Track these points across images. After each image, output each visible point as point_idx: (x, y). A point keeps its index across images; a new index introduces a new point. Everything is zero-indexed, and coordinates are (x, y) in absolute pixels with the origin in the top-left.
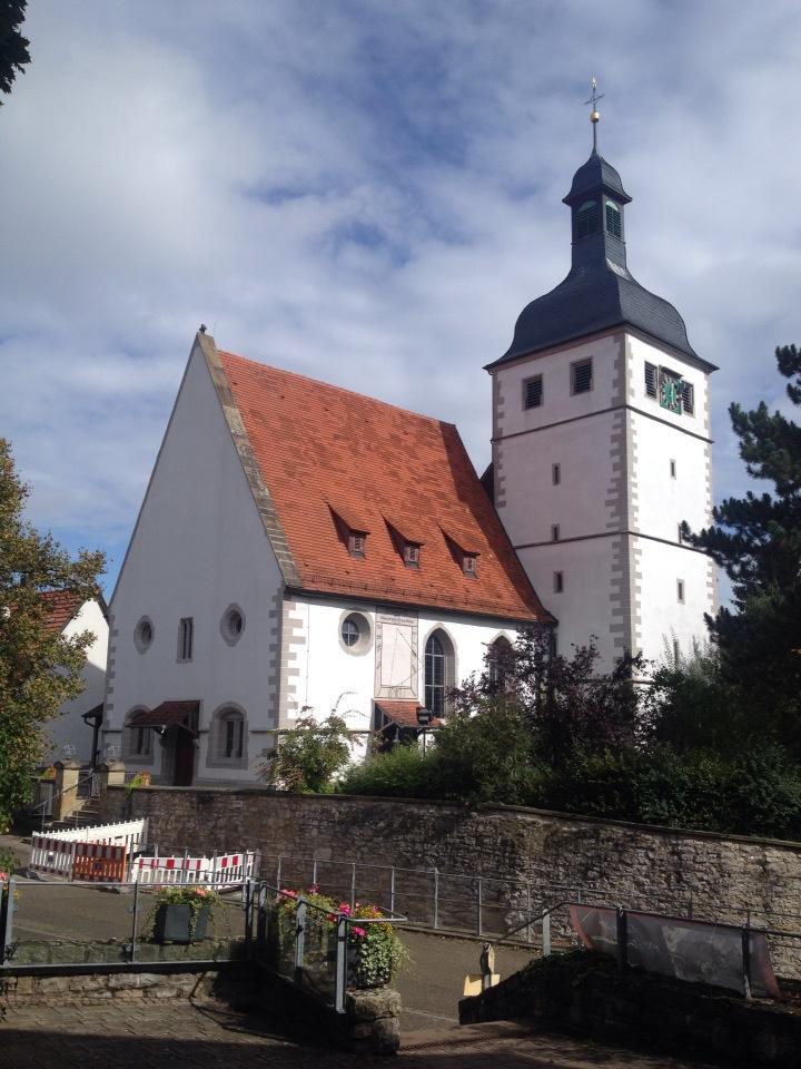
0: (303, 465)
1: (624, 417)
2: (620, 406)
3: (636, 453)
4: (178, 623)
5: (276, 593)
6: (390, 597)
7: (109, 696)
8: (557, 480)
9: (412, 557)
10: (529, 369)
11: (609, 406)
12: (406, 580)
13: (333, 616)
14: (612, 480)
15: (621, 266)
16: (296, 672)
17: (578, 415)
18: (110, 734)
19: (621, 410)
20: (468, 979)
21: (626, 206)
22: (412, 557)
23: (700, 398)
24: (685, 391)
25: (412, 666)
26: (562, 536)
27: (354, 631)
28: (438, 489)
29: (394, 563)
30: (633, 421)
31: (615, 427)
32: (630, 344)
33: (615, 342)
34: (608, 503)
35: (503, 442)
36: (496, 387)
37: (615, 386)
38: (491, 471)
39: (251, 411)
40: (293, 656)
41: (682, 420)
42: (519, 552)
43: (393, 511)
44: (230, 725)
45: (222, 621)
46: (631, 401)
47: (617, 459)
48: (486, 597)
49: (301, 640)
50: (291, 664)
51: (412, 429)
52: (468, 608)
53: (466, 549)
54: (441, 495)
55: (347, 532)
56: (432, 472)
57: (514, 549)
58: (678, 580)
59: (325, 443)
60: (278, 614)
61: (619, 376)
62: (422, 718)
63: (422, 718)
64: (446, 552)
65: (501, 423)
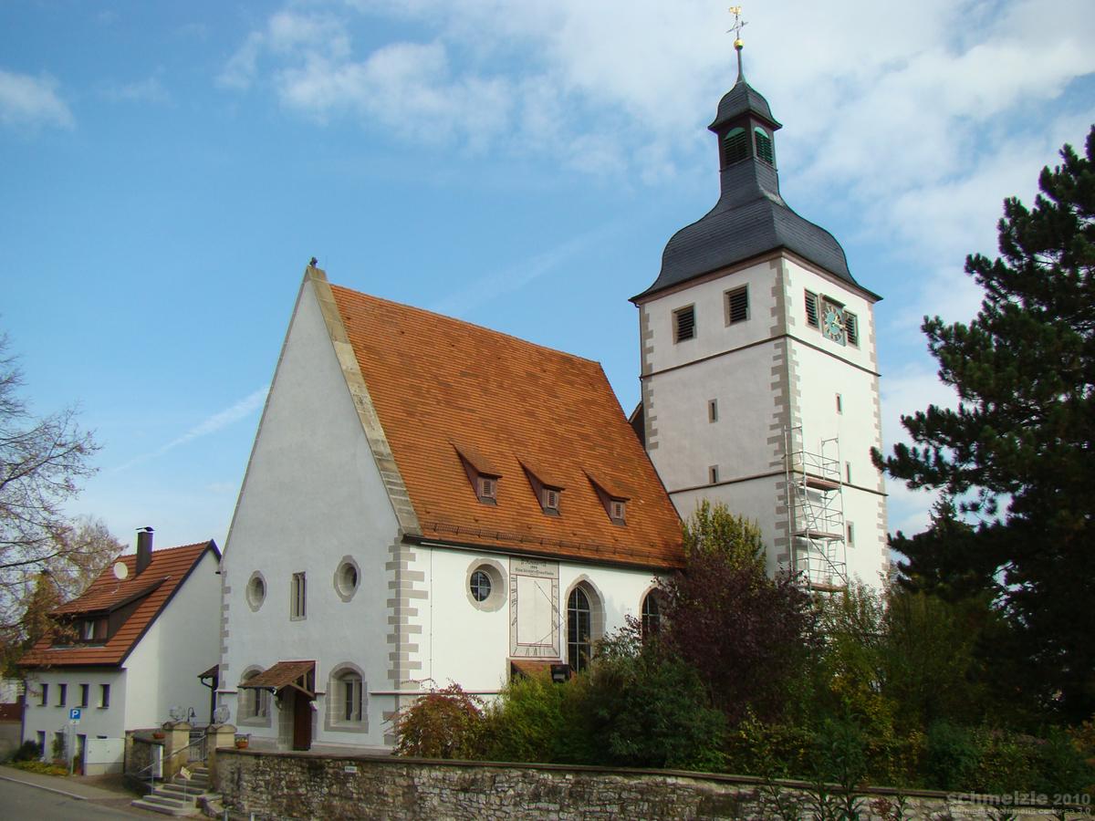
0: (423, 404)
1: (784, 347)
2: (780, 336)
3: (799, 386)
4: (290, 579)
5: (393, 544)
6: (525, 546)
7: (224, 655)
8: (714, 417)
9: (552, 503)
11: (769, 337)
12: (545, 529)
13: (459, 566)
14: (775, 416)
16: (418, 629)
18: (226, 695)
19: (782, 340)
20: (1038, 209)
21: (775, 132)
22: (552, 503)
23: (864, 329)
24: (849, 324)
25: (553, 622)
26: (721, 479)
27: (481, 585)
28: (583, 431)
29: (530, 509)
30: (795, 352)
31: (776, 358)
33: (771, 268)
34: (771, 440)
35: (654, 378)
36: (644, 320)
37: (773, 315)
38: (640, 413)
39: (366, 347)
40: (414, 612)
41: (846, 351)
42: (671, 496)
43: (529, 453)
44: (349, 686)
45: (335, 575)
46: (792, 331)
47: (778, 392)
48: (638, 546)
49: (423, 595)
50: (412, 621)
51: (552, 367)
52: (617, 558)
53: (614, 494)
54: (585, 437)
55: (475, 474)
56: (573, 411)
58: (853, 546)
59: (451, 380)
60: (394, 565)
61: (778, 302)
62: (556, 677)
63: (556, 677)
64: (592, 497)
65: (650, 358)
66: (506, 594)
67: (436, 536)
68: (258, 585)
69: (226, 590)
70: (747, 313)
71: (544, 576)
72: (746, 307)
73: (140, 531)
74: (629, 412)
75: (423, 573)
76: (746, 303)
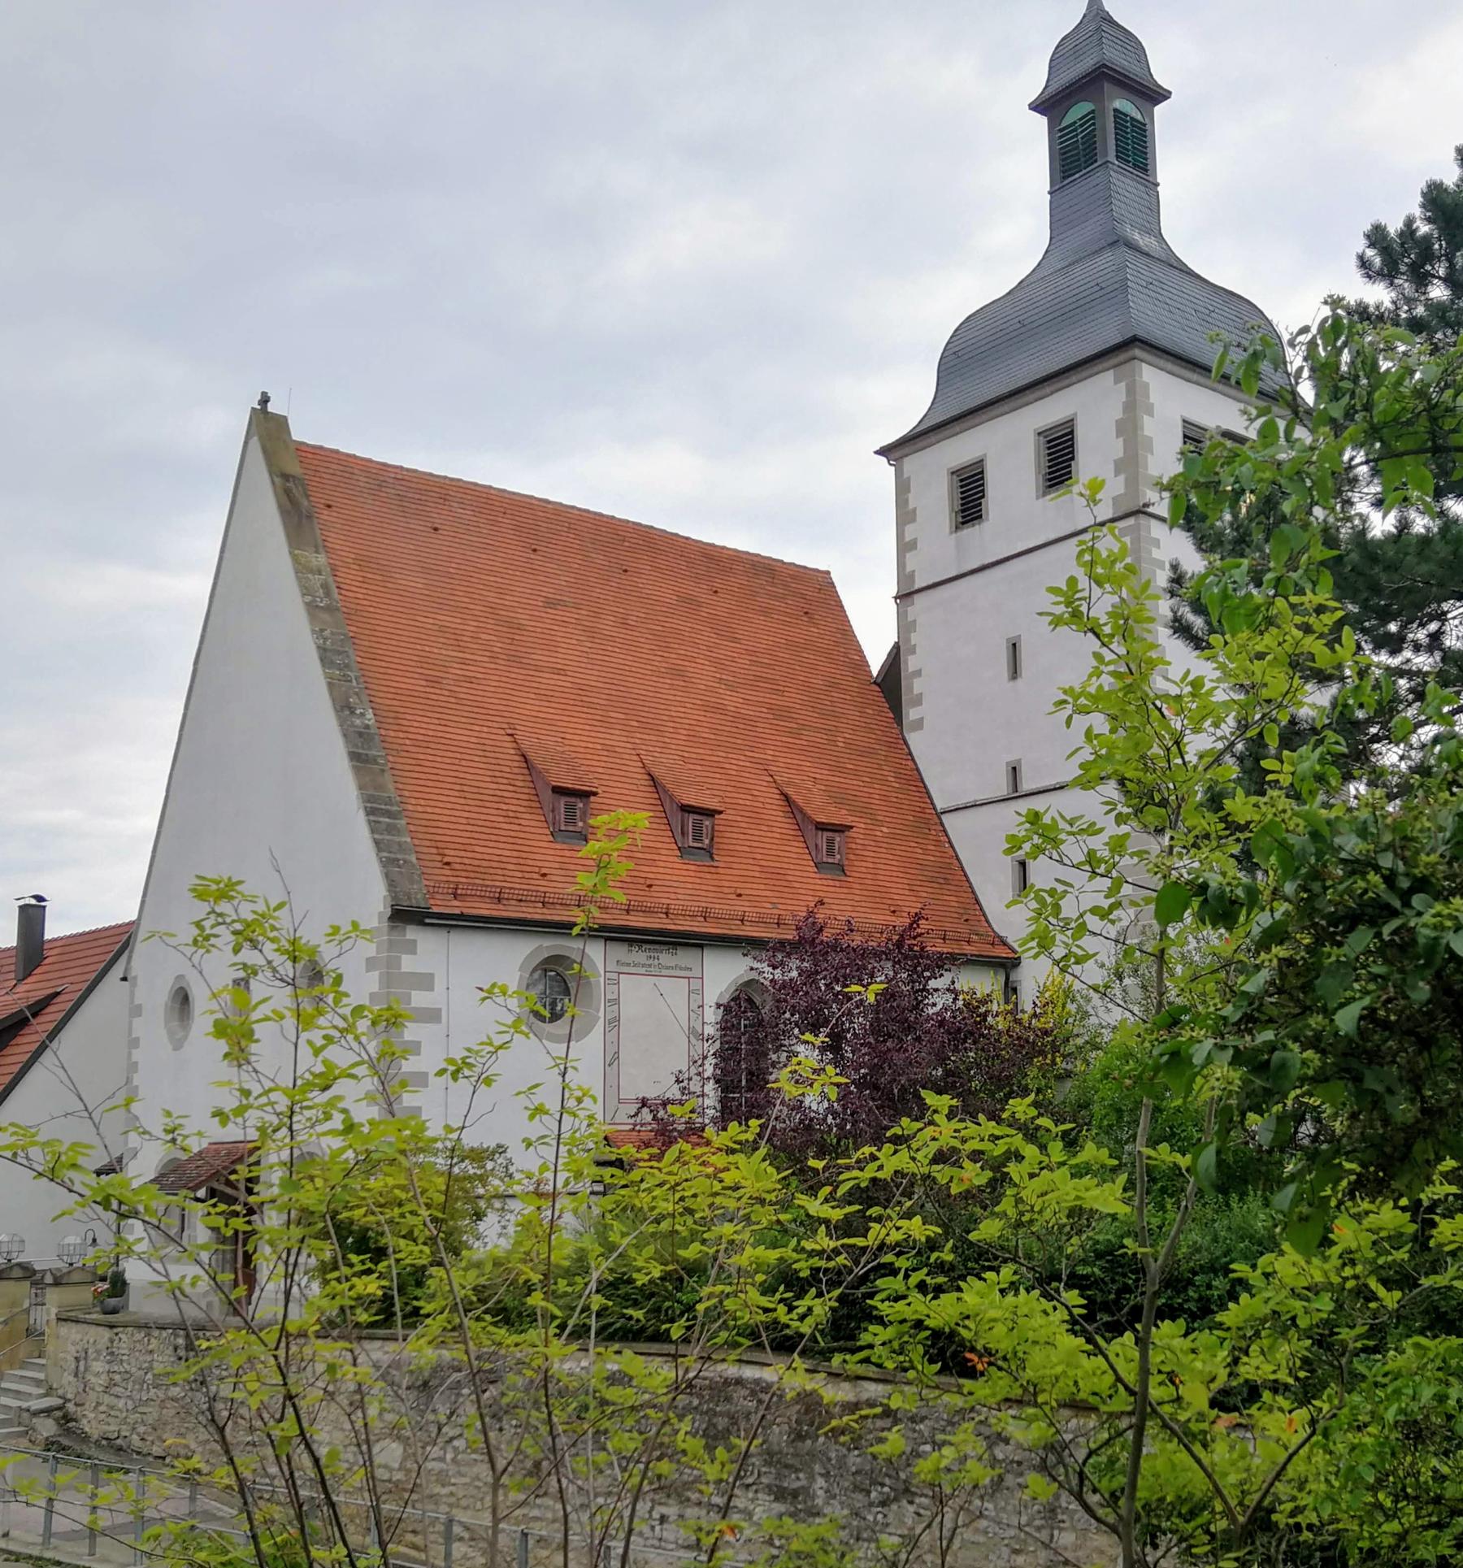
6: (636, 921)
10: (959, 450)
11: (1110, 516)
15: (1149, 232)
17: (1052, 537)
21: (1158, 110)
26: (1026, 785)
30: (1157, 543)
32: (1147, 385)
35: (916, 597)
36: (902, 488)
49: (432, 1016)
57: (939, 815)
66: (598, 1011)
67: (455, 906)
68: (182, 999)
69: (136, 1011)
70: (1073, 468)
71: (673, 973)
72: (1073, 459)
73: (22, 902)
74: (876, 661)
75: (432, 976)
76: (1072, 452)
